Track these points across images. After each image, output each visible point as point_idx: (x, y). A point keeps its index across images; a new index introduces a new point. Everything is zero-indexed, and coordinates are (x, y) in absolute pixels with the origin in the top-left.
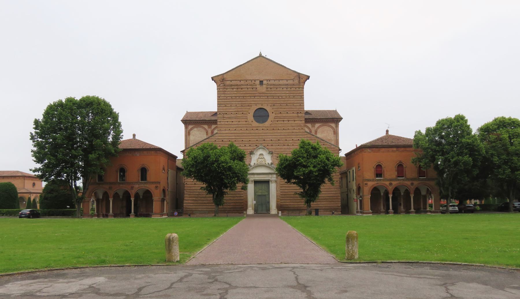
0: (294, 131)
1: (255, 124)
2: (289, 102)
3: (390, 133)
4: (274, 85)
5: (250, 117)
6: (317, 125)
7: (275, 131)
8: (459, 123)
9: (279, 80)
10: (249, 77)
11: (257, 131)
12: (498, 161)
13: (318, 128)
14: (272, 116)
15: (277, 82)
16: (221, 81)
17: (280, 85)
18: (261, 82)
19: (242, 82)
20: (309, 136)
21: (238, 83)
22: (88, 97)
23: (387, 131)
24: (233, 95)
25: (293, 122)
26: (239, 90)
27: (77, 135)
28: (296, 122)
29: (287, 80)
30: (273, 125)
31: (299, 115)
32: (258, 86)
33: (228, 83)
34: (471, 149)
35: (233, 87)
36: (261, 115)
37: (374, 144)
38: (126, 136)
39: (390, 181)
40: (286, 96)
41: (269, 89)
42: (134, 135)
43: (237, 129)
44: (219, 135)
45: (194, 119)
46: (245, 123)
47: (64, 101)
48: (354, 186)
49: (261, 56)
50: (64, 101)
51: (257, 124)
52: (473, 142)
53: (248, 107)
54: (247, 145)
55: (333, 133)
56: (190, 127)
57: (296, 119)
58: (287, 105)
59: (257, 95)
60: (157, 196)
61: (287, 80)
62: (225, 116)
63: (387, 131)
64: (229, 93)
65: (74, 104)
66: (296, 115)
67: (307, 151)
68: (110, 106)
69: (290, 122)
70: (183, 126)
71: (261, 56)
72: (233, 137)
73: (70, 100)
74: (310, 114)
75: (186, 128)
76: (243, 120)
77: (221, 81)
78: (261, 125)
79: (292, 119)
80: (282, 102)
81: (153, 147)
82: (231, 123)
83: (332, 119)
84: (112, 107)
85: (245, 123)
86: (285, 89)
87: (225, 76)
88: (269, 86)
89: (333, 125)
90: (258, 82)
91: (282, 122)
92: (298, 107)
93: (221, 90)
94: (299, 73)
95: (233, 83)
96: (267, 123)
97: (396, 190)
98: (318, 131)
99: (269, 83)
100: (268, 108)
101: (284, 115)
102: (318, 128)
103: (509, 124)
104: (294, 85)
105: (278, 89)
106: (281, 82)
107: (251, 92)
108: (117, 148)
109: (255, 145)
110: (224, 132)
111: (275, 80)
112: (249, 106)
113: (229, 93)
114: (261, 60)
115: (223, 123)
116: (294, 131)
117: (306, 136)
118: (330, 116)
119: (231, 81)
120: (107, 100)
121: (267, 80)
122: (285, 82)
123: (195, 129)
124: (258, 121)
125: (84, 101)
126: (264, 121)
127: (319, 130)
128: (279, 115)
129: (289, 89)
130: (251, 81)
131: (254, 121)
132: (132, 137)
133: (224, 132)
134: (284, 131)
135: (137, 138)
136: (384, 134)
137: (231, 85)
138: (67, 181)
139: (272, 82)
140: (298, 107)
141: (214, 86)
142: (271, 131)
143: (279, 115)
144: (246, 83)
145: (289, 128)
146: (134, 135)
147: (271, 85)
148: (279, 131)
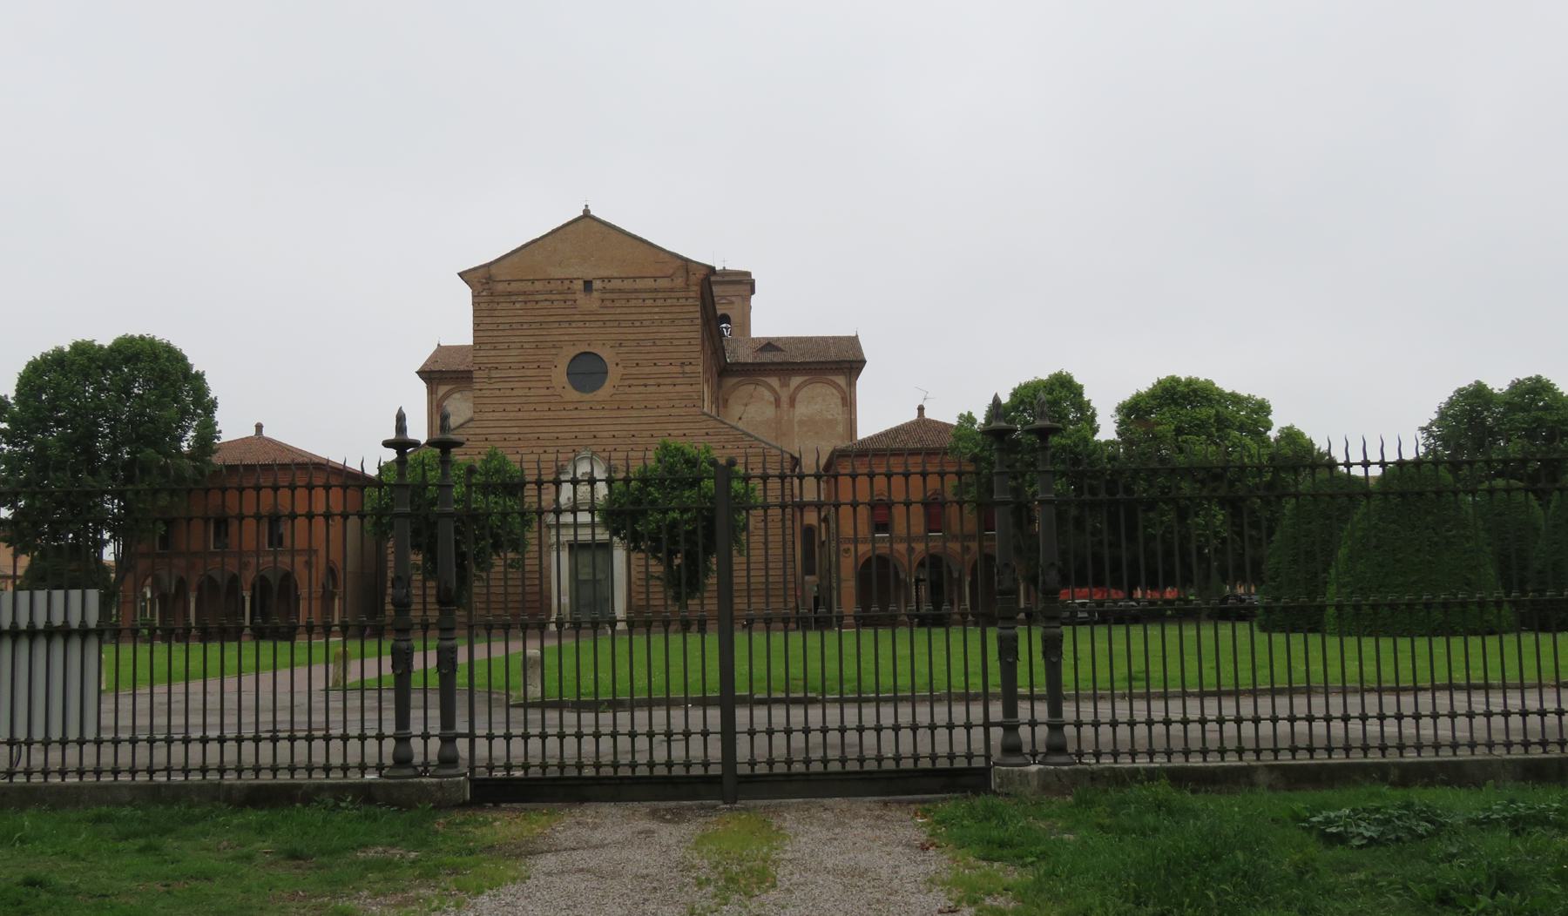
0: (673, 411)
1: (573, 395)
2: (660, 336)
3: (928, 415)
4: (620, 291)
5: (560, 376)
6: (796, 381)
7: (624, 413)
8: (1057, 399)
9: (634, 278)
10: (557, 273)
11: (575, 414)
12: (1145, 491)
13: (799, 388)
14: (614, 375)
15: (628, 285)
16: (482, 280)
17: (636, 291)
18: (588, 285)
19: (538, 286)
20: (712, 423)
21: (528, 287)
22: (130, 340)
23: (921, 409)
24: (517, 319)
25: (670, 388)
26: (529, 305)
27: (115, 425)
28: (678, 388)
29: (655, 279)
30: (617, 398)
31: (687, 369)
32: (580, 296)
33: (501, 287)
34: (1082, 460)
35: (514, 298)
36: (587, 371)
37: (876, 446)
38: (232, 426)
39: (909, 539)
40: (653, 321)
41: (608, 303)
42: (259, 427)
43: (526, 407)
44: (478, 424)
45: (454, 368)
46: (545, 392)
47: (67, 349)
48: (1193, 547)
49: (587, 214)
50: (67, 349)
51: (575, 395)
52: (1076, 445)
53: (554, 351)
54: (550, 450)
55: (839, 401)
56: (442, 390)
57: (678, 381)
58: (654, 344)
59: (576, 318)
60: (308, 584)
61: (655, 279)
62: (494, 374)
63: (921, 409)
64: (503, 313)
65: (92, 360)
66: (679, 369)
67: (671, 469)
68: (184, 358)
69: (663, 389)
70: (422, 386)
71: (587, 214)
72: (515, 430)
73: (81, 349)
74: (777, 349)
75: (431, 392)
76: (540, 384)
77: (482, 280)
78: (587, 397)
79: (668, 381)
80: (642, 336)
81: (300, 460)
82: (508, 393)
83: (838, 363)
84: (190, 361)
85: (545, 392)
86: (649, 302)
87: (494, 270)
88: (607, 296)
89: (841, 380)
90: (579, 285)
91: (642, 389)
92: (683, 349)
93: (483, 306)
94: (687, 260)
95: (514, 287)
96: (604, 392)
97: (934, 562)
98: (800, 396)
99: (609, 286)
100: (606, 354)
101: (647, 370)
102: (799, 388)
103: (1185, 397)
104: (672, 290)
105: (633, 303)
106: (640, 284)
107: (561, 311)
108: (209, 463)
109: (569, 449)
110: (489, 416)
111: (622, 279)
112: (554, 347)
113: (503, 313)
114: (587, 230)
115: (487, 393)
116: (673, 411)
117: (703, 425)
118: (833, 355)
119: (509, 282)
120: (177, 344)
121: (603, 279)
122: (650, 283)
123: (457, 396)
124: (578, 387)
125: (120, 352)
126: (594, 388)
127: (801, 395)
128: (634, 371)
129: (659, 302)
130: (562, 280)
131: (568, 387)
132: (252, 432)
133: (489, 416)
134: (648, 413)
135: (266, 433)
136: (914, 416)
137: (510, 294)
138: (75, 549)
139: (616, 284)
140: (683, 349)
141: (467, 292)
142: (614, 414)
143: (634, 371)
144: (549, 287)
145: (660, 403)
146: (259, 427)
147: (612, 291)
148: (634, 413)
